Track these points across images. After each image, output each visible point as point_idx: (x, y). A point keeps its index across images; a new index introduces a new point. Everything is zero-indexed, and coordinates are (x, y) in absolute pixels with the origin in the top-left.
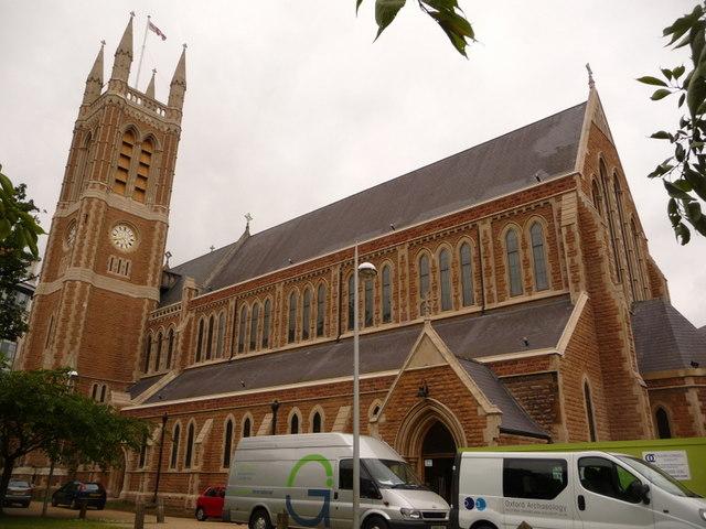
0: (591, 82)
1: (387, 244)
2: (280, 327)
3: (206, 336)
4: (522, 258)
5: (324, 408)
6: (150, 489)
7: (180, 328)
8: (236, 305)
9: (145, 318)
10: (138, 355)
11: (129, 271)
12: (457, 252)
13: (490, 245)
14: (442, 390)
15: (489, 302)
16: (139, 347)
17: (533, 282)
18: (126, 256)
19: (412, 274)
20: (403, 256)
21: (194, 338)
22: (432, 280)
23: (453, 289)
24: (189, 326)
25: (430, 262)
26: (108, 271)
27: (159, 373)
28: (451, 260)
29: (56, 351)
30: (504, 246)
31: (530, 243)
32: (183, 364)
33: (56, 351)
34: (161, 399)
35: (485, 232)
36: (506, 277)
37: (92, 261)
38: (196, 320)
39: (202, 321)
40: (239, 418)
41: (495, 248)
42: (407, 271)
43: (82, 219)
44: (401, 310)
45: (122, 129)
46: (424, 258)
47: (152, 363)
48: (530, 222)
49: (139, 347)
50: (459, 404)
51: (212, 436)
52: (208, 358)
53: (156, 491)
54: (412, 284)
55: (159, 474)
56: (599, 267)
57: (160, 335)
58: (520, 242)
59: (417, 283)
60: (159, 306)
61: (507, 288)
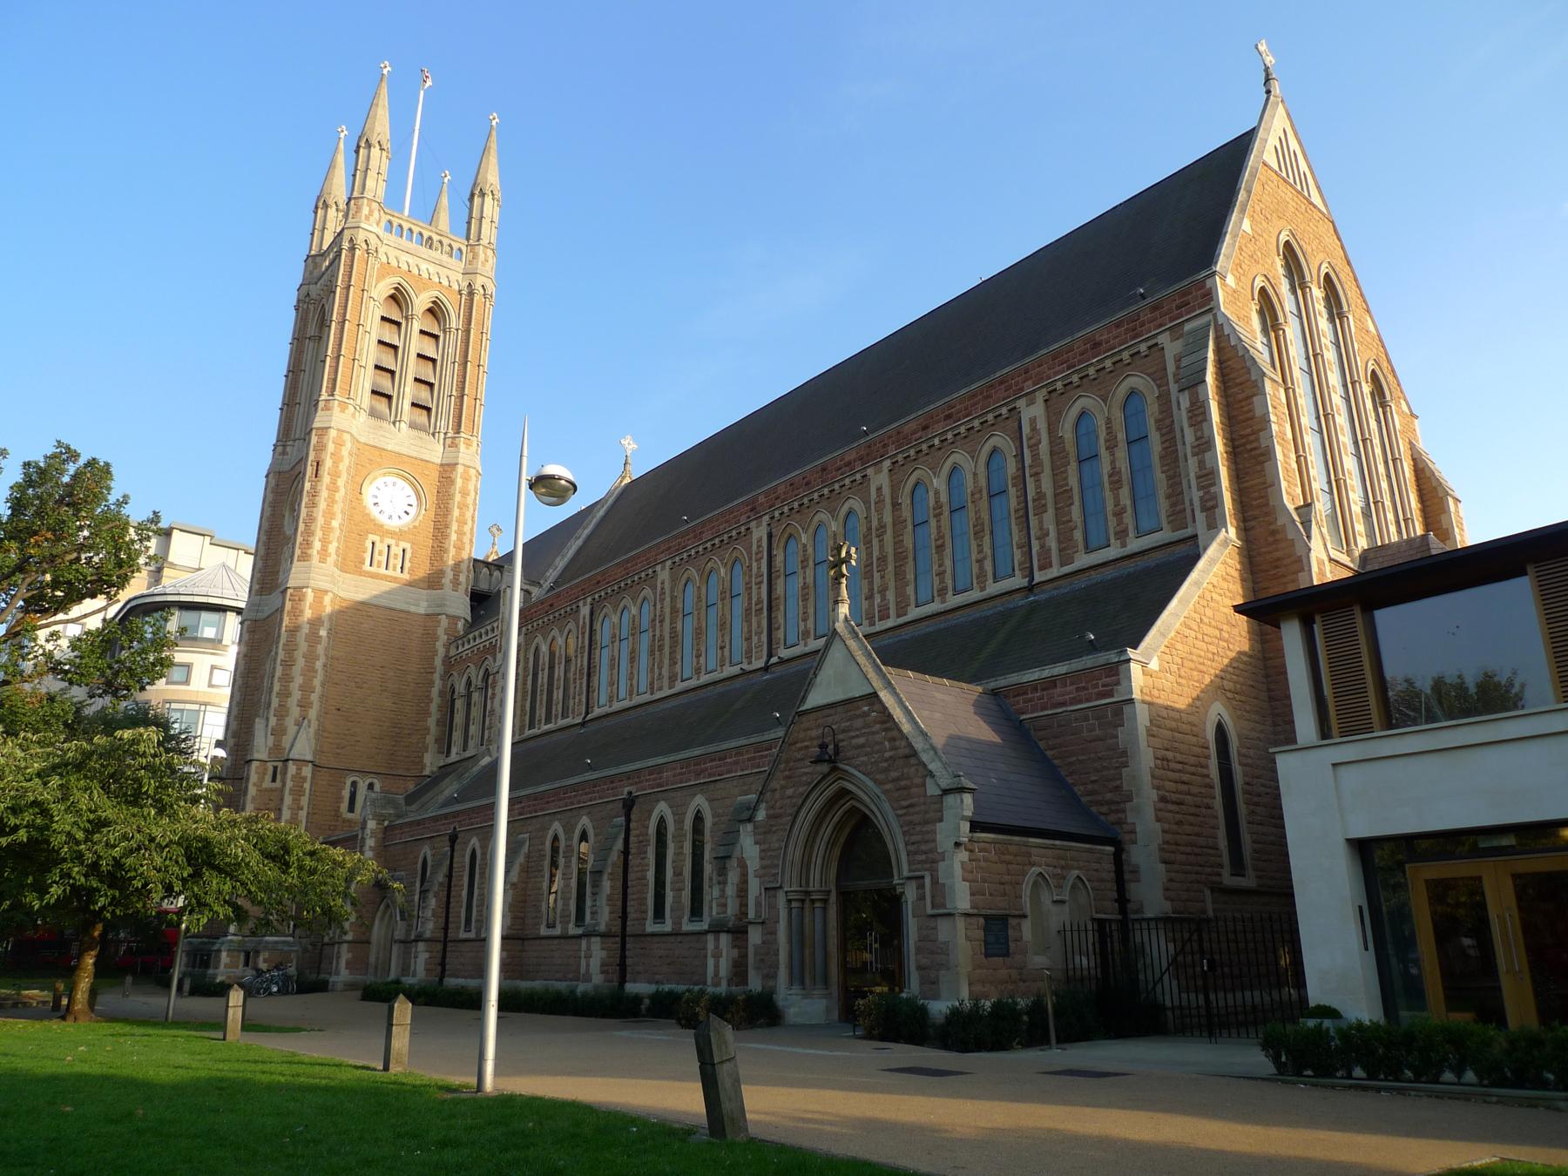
3: (543, 677)
4: (1106, 468)
5: (710, 801)
8: (592, 614)
9: (441, 651)
10: (432, 722)
11: (407, 565)
12: (982, 469)
13: (1044, 447)
14: (862, 746)
15: (1041, 568)
16: (434, 707)
17: (1128, 518)
18: (399, 535)
19: (898, 523)
20: (879, 489)
22: (934, 531)
23: (974, 548)
25: (931, 494)
26: (367, 566)
27: (468, 754)
31: (1121, 436)
33: (273, 721)
35: (1033, 421)
36: (1076, 512)
37: (332, 548)
39: (537, 649)
40: (569, 830)
41: (1052, 453)
42: (888, 518)
44: (877, 599)
45: (382, 289)
46: (920, 491)
47: (457, 736)
48: (1122, 391)
50: (894, 774)
52: (548, 720)
54: (898, 543)
58: (1103, 435)
59: (908, 541)
61: (1078, 535)
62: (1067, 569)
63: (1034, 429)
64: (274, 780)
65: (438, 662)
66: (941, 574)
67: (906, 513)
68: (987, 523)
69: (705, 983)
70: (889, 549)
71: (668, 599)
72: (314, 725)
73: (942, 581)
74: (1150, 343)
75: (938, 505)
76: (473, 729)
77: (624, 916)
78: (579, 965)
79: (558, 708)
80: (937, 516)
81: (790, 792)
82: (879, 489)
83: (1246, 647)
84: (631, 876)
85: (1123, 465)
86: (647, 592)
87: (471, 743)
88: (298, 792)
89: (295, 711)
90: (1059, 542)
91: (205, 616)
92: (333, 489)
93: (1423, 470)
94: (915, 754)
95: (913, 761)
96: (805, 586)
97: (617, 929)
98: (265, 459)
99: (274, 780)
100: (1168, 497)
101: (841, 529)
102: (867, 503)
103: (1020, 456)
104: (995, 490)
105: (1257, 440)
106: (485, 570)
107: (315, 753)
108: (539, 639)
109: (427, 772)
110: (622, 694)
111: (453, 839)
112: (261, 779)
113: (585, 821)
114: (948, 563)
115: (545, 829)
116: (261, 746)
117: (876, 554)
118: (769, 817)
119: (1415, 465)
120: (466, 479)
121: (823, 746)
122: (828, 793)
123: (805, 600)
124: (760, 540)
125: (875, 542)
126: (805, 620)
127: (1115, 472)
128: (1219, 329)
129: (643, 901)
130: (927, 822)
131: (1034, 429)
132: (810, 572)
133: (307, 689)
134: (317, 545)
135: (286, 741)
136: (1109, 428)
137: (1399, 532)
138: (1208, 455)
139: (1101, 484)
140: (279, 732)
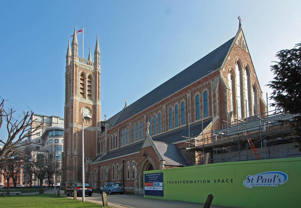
0: (240, 25)
1: (159, 105)
2: (131, 137)
4: (200, 105)
6: (97, 186)
7: (106, 139)
10: (96, 148)
16: (96, 146)
19: (167, 115)
20: (164, 109)
21: (110, 142)
22: (173, 116)
23: (179, 120)
24: (108, 139)
28: (178, 109)
29: (70, 149)
30: (195, 102)
31: (203, 100)
32: (108, 150)
33: (70, 149)
34: (100, 161)
35: (189, 97)
38: (110, 137)
39: (112, 137)
40: (115, 165)
43: (71, 107)
44: (163, 128)
45: (79, 73)
47: (101, 150)
48: (204, 91)
49: (96, 146)
50: (154, 158)
51: (110, 171)
52: (114, 148)
53: (99, 187)
54: (167, 118)
55: (124, 181)
56: (224, 106)
57: (102, 142)
60: (101, 133)
62: (193, 123)
63: (189, 98)
64: (71, 158)
65: (97, 139)
66: (173, 124)
67: (168, 113)
68: (181, 115)
69: (133, 186)
70: (165, 120)
71: (165, 112)
72: (77, 149)
73: (174, 125)
74: (209, 82)
75: (173, 112)
76: (103, 149)
77: (124, 178)
78: (134, 185)
79: (115, 146)
80: (173, 114)
81: (140, 160)
82: (164, 109)
83: (167, 146)
84: (289, 161)
85: (203, 105)
86: (128, 127)
87: (103, 152)
88: (75, 160)
89: (74, 147)
90: (192, 118)
91: (60, 132)
92: (76, 110)
93: (262, 103)
94: (157, 155)
95: (157, 156)
96: (152, 126)
97: (122, 179)
98: (63, 105)
99: (71, 158)
100: (210, 110)
101: (158, 116)
102: (162, 111)
103: (187, 103)
104: (197, 103)
105: (224, 100)
106: (103, 123)
107: (78, 154)
108: (112, 135)
109: (96, 156)
110: (125, 144)
111: (99, 167)
112: (69, 158)
113: (118, 164)
114: (175, 122)
115: (112, 165)
116: (69, 153)
117: (163, 120)
118: (138, 164)
119: (260, 101)
120: (99, 108)
121: (144, 154)
122: (146, 160)
123: (152, 128)
124: (145, 118)
125: (163, 118)
126: (152, 131)
127: (201, 106)
128: (220, 79)
129: (126, 176)
130: (158, 165)
131: (189, 98)
132: (153, 123)
133: (75, 144)
134: (74, 120)
135: (73, 152)
136: (201, 98)
137: (250, 113)
138: (215, 103)
139: (199, 108)
140: (71, 151)
